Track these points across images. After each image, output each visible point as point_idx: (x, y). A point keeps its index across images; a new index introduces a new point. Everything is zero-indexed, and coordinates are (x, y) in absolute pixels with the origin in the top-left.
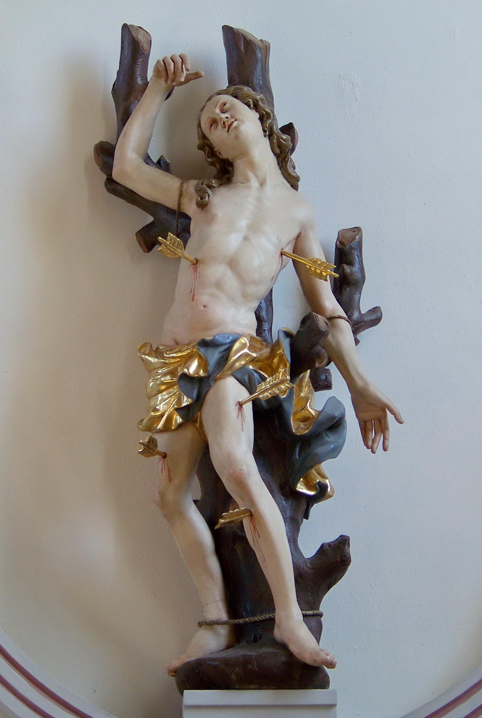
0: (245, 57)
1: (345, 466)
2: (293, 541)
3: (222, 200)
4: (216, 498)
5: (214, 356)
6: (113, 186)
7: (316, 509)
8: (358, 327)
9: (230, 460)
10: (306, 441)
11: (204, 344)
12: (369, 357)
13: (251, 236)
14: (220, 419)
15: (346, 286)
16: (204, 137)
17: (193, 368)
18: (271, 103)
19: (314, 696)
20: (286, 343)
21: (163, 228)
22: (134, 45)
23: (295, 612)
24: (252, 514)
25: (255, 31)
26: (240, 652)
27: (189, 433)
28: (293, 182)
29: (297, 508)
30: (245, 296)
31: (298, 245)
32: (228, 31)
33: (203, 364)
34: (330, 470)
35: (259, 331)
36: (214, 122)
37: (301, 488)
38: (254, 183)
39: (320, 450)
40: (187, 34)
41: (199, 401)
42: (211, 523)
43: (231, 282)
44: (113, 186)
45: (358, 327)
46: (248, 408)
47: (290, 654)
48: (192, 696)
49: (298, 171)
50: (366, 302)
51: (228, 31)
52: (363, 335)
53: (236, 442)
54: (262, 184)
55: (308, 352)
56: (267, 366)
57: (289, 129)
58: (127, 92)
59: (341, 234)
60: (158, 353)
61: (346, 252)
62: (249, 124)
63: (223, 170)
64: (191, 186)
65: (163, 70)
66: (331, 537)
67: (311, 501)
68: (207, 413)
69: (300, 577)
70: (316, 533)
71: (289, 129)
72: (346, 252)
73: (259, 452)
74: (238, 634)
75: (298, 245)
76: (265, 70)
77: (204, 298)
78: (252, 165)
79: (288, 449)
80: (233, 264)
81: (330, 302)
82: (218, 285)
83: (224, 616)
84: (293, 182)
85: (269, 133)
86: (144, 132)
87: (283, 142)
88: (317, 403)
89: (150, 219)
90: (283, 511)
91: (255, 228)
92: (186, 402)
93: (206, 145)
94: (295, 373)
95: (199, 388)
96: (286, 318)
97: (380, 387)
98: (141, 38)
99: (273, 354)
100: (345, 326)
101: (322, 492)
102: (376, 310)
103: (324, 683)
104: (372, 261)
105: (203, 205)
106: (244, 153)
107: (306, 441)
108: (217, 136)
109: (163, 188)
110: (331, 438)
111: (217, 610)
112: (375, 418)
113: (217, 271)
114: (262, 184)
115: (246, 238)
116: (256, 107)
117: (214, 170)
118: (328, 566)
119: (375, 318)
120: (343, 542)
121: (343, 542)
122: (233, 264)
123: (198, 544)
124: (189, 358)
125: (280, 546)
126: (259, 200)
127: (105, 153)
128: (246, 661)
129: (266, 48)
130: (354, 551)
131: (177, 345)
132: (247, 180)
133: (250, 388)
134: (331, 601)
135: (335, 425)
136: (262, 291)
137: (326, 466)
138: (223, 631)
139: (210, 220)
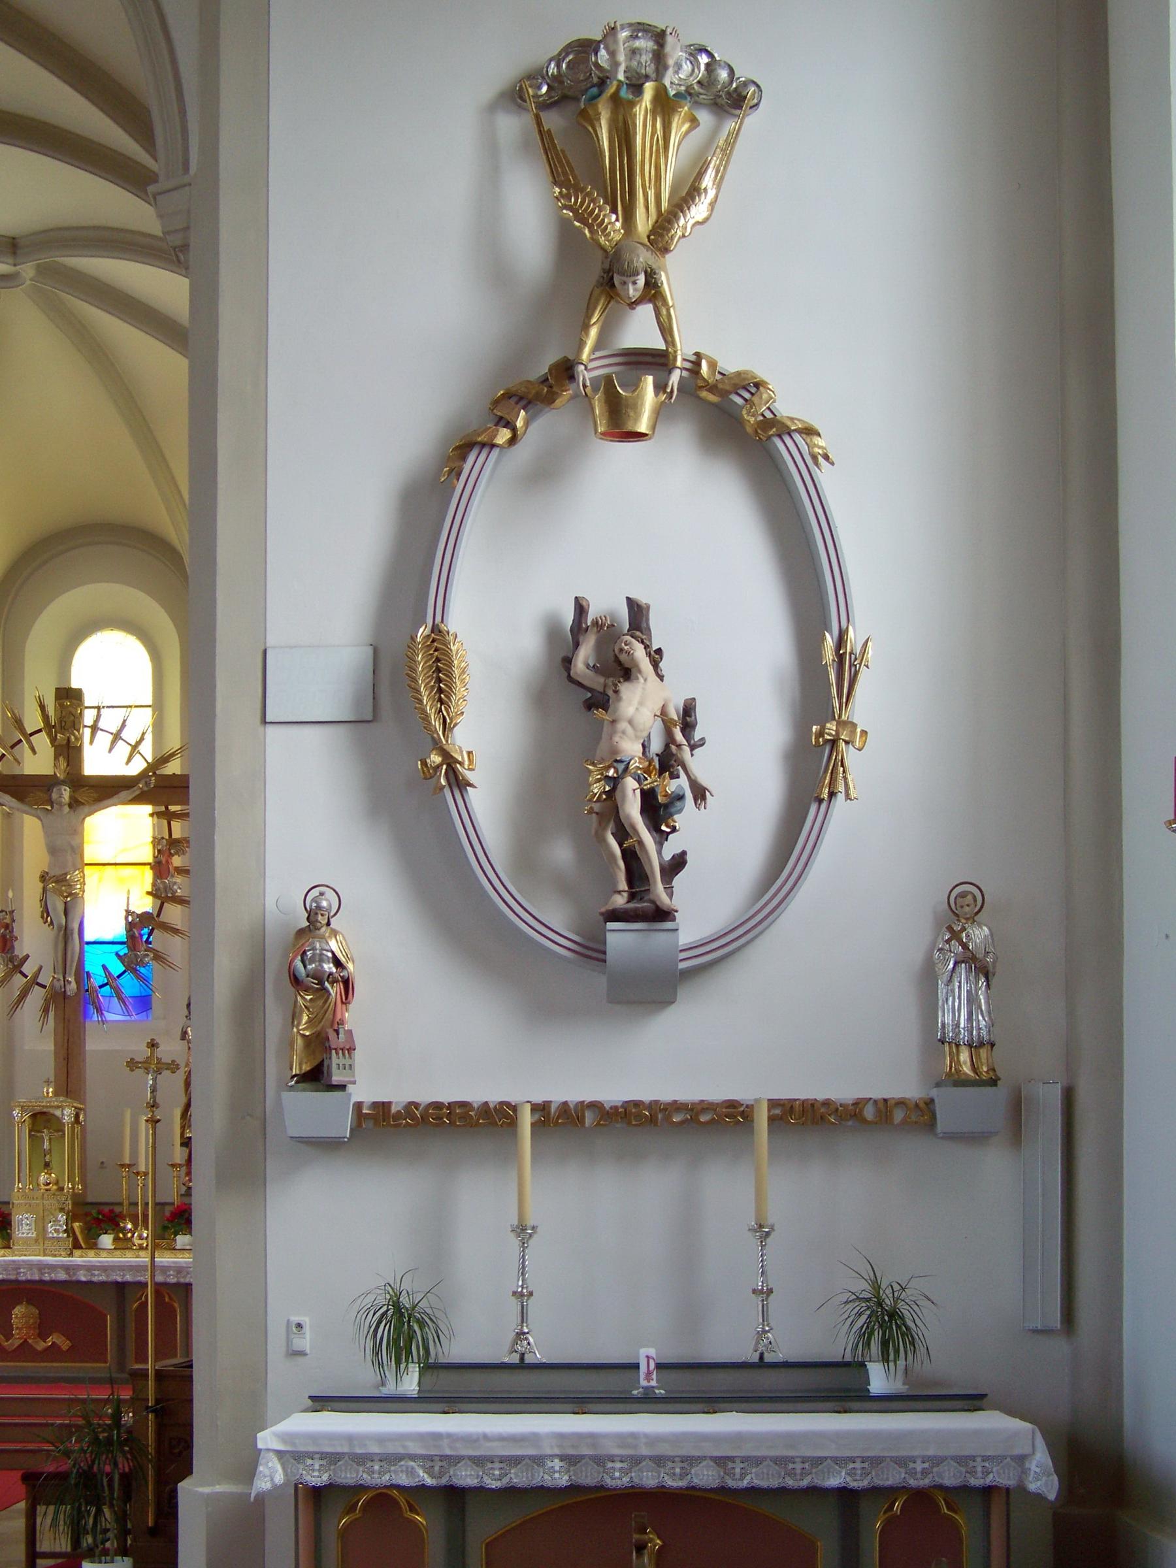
0: (637, 612)
1: (687, 817)
2: (659, 852)
3: (625, 689)
4: (623, 833)
5: (621, 767)
6: (570, 679)
7: (671, 836)
8: (693, 748)
9: (628, 817)
10: (666, 806)
11: (616, 761)
12: (699, 764)
13: (640, 708)
14: (624, 796)
15: (688, 726)
16: (616, 656)
17: (611, 773)
18: (650, 640)
19: (669, 925)
20: (656, 760)
21: (599, 702)
22: (581, 608)
23: (660, 887)
24: (641, 842)
25: (642, 598)
26: (631, 905)
27: (609, 803)
28: (661, 678)
29: (662, 837)
30: (637, 737)
31: (664, 712)
32: (628, 598)
33: (616, 771)
34: (679, 820)
35: (644, 753)
36: (621, 650)
37: (664, 828)
38: (642, 680)
39: (673, 810)
40: (607, 603)
41: (614, 789)
42: (620, 845)
43: (629, 730)
44: (570, 679)
45: (693, 748)
46: (638, 792)
47: (657, 907)
48: (611, 925)
49: (664, 673)
50: (697, 736)
51: (628, 598)
52: (696, 751)
53: (633, 808)
54: (645, 680)
55: (667, 763)
56: (647, 771)
57: (659, 651)
58: (579, 628)
59: (686, 701)
60: (593, 764)
61: (688, 710)
62: (639, 652)
63: (627, 672)
64: (610, 681)
65: (595, 623)
66: (679, 851)
67: (668, 834)
68: (618, 794)
69: (663, 870)
70: (670, 849)
71: (659, 651)
72: (688, 710)
73: (643, 811)
74: (632, 897)
75: (664, 712)
76: (647, 620)
77: (616, 738)
78: (640, 671)
79: (657, 811)
80: (630, 722)
81: (679, 736)
82: (624, 732)
83: (626, 888)
84: (661, 678)
85: (649, 655)
86: (585, 655)
87: (656, 657)
88: (672, 786)
89: (589, 695)
90: (654, 838)
91: (641, 703)
92: (607, 788)
93: (617, 661)
94: (660, 774)
95: (615, 782)
96: (656, 746)
97: (703, 780)
98: (584, 604)
99: (650, 765)
100: (687, 749)
101: (674, 830)
102: (703, 739)
103: (674, 919)
104: (700, 713)
105: (616, 692)
106: (637, 666)
107: (666, 806)
108: (623, 657)
109: (596, 682)
110: (678, 804)
111: (623, 885)
112: (700, 794)
113: (623, 725)
114: (645, 680)
115: (637, 709)
116: (642, 642)
117: (622, 673)
118: (678, 863)
119: (702, 742)
120: (684, 853)
121: (684, 853)
122: (630, 722)
123: (612, 855)
124: (608, 768)
125: (654, 855)
126: (644, 689)
127: (567, 662)
128: (636, 909)
129: (648, 607)
130: (688, 858)
131: (602, 761)
132: (637, 679)
133: (639, 781)
134: (678, 881)
135: (681, 798)
136: (645, 734)
137: (676, 817)
138: (625, 895)
139: (619, 699)
